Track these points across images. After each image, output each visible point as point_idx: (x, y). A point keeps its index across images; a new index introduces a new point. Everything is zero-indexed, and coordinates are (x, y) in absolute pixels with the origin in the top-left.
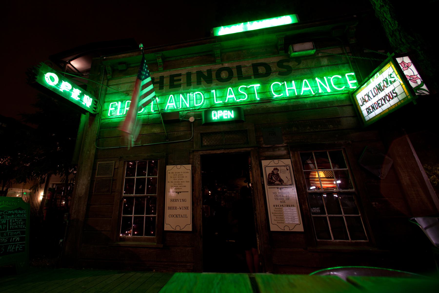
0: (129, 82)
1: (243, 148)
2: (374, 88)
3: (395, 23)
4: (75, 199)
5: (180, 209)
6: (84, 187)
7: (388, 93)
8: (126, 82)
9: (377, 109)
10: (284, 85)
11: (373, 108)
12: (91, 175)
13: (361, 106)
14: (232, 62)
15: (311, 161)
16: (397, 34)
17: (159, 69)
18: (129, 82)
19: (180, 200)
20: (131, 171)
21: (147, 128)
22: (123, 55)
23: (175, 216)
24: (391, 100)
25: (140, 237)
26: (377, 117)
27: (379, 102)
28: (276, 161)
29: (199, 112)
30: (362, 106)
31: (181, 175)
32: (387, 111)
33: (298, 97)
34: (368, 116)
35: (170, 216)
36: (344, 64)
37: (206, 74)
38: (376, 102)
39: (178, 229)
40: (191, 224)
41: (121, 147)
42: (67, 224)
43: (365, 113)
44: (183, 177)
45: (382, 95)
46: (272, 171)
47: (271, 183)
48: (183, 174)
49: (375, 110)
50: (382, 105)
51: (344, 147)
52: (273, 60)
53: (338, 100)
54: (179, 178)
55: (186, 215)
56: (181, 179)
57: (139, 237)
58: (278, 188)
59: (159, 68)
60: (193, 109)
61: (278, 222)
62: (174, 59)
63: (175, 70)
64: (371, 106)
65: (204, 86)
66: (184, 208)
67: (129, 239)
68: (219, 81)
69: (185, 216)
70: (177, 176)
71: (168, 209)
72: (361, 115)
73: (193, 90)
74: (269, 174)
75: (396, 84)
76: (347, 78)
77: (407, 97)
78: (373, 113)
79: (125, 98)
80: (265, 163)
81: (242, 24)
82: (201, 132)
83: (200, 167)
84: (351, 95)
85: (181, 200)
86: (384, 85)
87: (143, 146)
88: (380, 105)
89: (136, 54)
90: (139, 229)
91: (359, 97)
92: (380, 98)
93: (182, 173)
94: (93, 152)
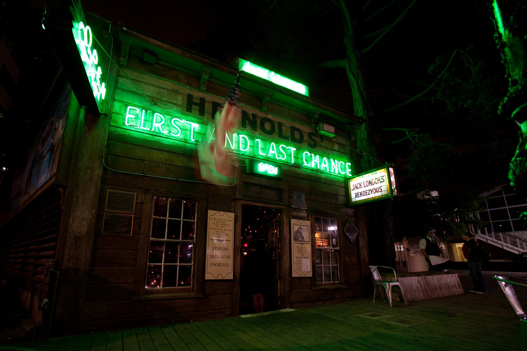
0: (156, 86)
1: (278, 205)
2: (367, 181)
3: (365, 133)
4: (67, 239)
5: (223, 257)
6: (84, 223)
7: (376, 188)
8: (150, 83)
9: (364, 195)
10: (311, 156)
11: (361, 194)
12: (96, 207)
13: (351, 190)
14: (275, 115)
15: (318, 225)
16: (364, 142)
17: (201, 88)
18: (156, 85)
19: (222, 248)
20: (160, 210)
21: (183, 159)
22: (158, 43)
23: (217, 265)
24: (376, 192)
25: (173, 288)
26: (362, 201)
27: (367, 192)
28: (301, 221)
29: (243, 158)
30: (352, 190)
31: (224, 222)
32: (371, 199)
33: (318, 171)
34: (354, 198)
35: (212, 265)
36: (346, 154)
37: (251, 118)
38: (365, 191)
39: (220, 278)
40: (233, 273)
41: (146, 175)
42: (58, 276)
43: (353, 196)
44: (226, 225)
45: (371, 187)
46: (298, 229)
47: (296, 239)
48: (226, 221)
49: (362, 196)
50: (369, 194)
51: (338, 218)
52: (306, 129)
53: (340, 181)
54: (221, 226)
55: (228, 264)
56: (223, 227)
57: (171, 289)
58: (300, 243)
59: (202, 87)
60: (237, 152)
61: (298, 270)
62: (219, 83)
63: (219, 97)
64: (360, 192)
65: (248, 131)
66: (226, 256)
67: (158, 292)
68: (263, 131)
69: (227, 265)
70: (220, 223)
71: (210, 258)
72: (350, 196)
73: (238, 131)
74: (296, 231)
75: (383, 184)
76: (347, 167)
77: (388, 194)
78: (360, 198)
79: (150, 107)
80: (293, 221)
81: (268, 70)
82: (244, 180)
83: (241, 216)
84: (347, 180)
85: (224, 249)
86: (375, 182)
87: (178, 180)
88: (367, 194)
89: (179, 52)
90: (169, 281)
91: (353, 183)
92: (369, 189)
93: (225, 220)
94: (99, 172)
